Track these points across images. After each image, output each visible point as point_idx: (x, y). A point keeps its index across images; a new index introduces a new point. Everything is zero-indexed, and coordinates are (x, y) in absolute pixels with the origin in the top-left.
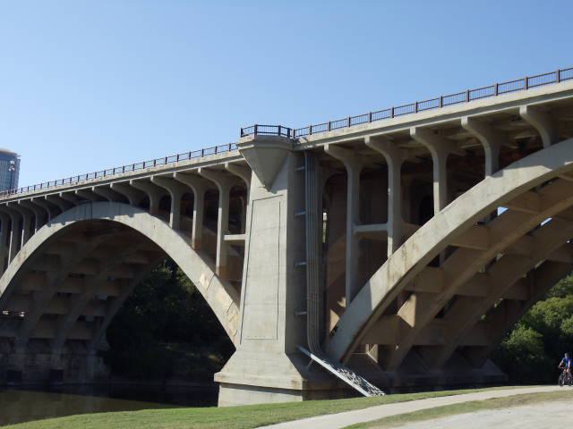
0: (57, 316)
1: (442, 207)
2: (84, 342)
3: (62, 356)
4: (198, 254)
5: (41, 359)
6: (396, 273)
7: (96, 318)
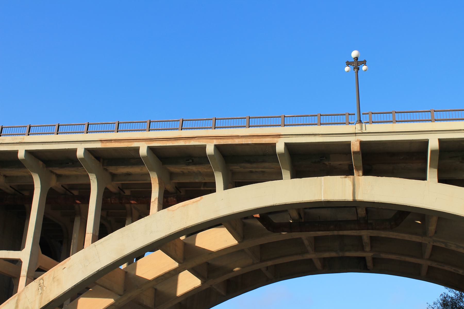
1: (94, 240)
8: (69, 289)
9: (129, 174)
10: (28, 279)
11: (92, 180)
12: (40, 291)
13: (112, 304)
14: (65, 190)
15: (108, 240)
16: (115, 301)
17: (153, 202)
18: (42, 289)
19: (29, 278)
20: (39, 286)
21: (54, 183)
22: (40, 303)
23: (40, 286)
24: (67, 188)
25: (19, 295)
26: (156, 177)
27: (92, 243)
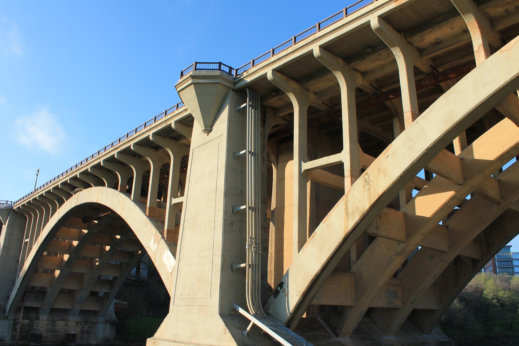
0: (74, 291)
1: (415, 117)
2: (95, 313)
3: (77, 323)
4: (151, 220)
5: (60, 325)
6: (357, 207)
7: (105, 293)
8: (398, 177)
9: (437, 43)
10: (353, 178)
11: (396, 55)
12: (367, 187)
13: (453, 196)
14: (374, 89)
15: (431, 111)
16: (455, 192)
17: (477, 51)
18: (369, 184)
19: (354, 177)
20: (364, 182)
21: (360, 81)
22: (370, 200)
23: (366, 182)
24: (377, 88)
25: (346, 196)
26: (474, 20)
27: (413, 122)
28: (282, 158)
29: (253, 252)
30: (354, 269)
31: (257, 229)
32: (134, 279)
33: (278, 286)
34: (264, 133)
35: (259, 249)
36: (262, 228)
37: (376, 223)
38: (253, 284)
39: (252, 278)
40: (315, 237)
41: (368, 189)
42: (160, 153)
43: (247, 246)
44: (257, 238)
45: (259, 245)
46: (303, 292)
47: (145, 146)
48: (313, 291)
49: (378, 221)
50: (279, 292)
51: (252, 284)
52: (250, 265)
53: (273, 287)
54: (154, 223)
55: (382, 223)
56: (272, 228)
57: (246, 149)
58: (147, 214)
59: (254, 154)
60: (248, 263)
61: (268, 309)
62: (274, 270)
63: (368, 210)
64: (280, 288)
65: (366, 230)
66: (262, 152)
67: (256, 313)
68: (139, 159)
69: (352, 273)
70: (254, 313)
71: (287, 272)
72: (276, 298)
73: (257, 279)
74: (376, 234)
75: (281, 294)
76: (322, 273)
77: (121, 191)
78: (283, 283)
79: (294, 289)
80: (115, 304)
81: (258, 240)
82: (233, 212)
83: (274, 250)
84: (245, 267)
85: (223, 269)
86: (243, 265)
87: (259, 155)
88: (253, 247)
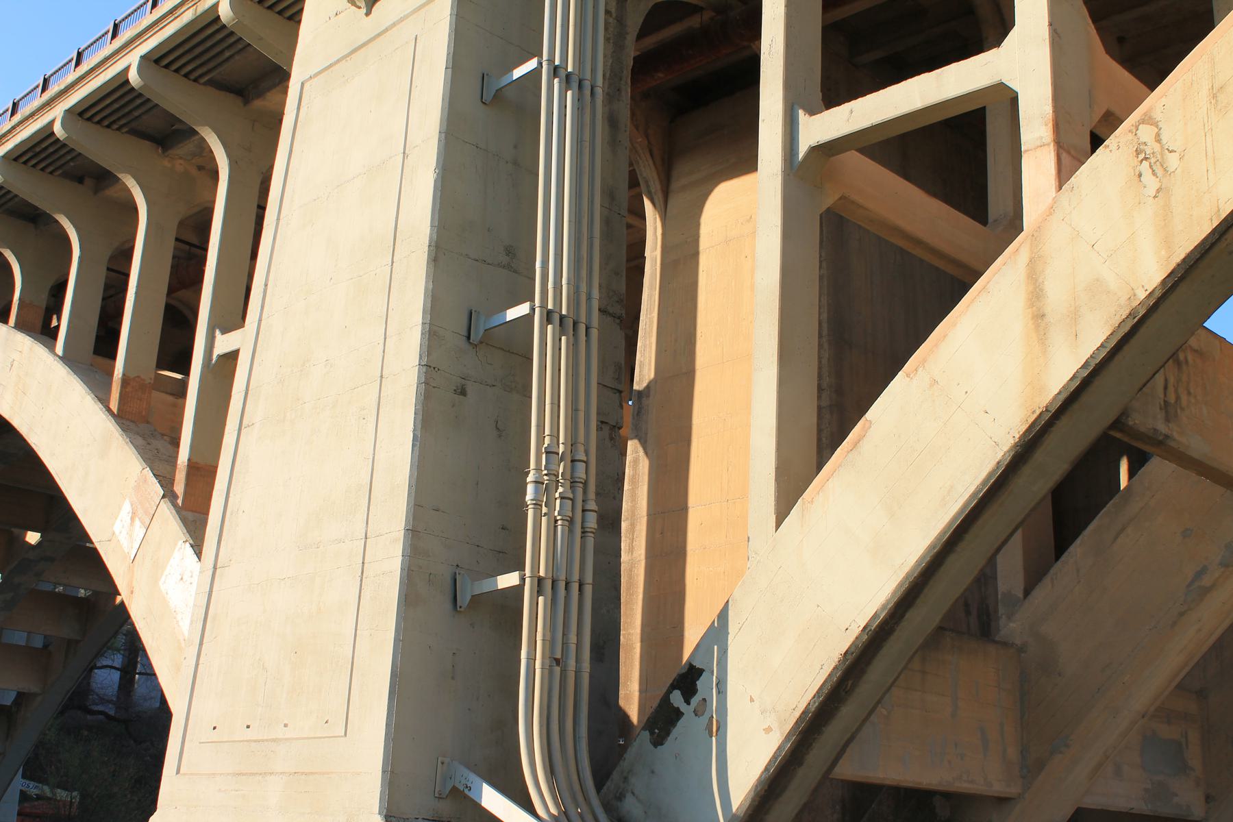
4: (125, 429)
19: (1069, 153)
20: (1136, 161)
23: (1146, 159)
28: (685, 172)
29: (559, 522)
30: (1012, 627)
31: (581, 415)
32: (112, 713)
33: (673, 687)
34: (620, 21)
35: (588, 507)
36: (602, 423)
37: (1166, 388)
38: (551, 673)
39: (550, 643)
40: (866, 446)
41: (1158, 191)
42: (179, 159)
43: (530, 489)
44: (577, 458)
45: (585, 492)
46: (797, 714)
47: (115, 126)
48: (848, 712)
49: (1172, 380)
50: (678, 714)
51: (546, 672)
52: (540, 580)
53: (634, 718)
54: (140, 441)
55: (1189, 393)
56: (636, 461)
57: (532, 300)
58: (114, 406)
59: (548, 584)
60: (532, 571)
61: (620, 797)
62: (642, 641)
63: (1158, 294)
64: (683, 694)
65: (1125, 413)
66: (608, 94)
67: (565, 813)
68: (97, 190)
69: (1005, 644)
70: (553, 811)
71: (719, 616)
72: (662, 744)
73: (573, 647)
74: (1167, 437)
75: (688, 725)
76: (897, 623)
77: (21, 326)
78: (700, 672)
79: (752, 700)
80: (24, 797)
81: (581, 467)
82: (469, 337)
83: (643, 557)
84: (518, 590)
85: (409, 598)
86: (507, 580)
87: (599, 91)
88: (557, 495)
